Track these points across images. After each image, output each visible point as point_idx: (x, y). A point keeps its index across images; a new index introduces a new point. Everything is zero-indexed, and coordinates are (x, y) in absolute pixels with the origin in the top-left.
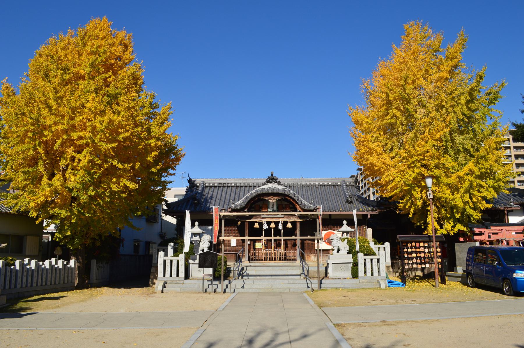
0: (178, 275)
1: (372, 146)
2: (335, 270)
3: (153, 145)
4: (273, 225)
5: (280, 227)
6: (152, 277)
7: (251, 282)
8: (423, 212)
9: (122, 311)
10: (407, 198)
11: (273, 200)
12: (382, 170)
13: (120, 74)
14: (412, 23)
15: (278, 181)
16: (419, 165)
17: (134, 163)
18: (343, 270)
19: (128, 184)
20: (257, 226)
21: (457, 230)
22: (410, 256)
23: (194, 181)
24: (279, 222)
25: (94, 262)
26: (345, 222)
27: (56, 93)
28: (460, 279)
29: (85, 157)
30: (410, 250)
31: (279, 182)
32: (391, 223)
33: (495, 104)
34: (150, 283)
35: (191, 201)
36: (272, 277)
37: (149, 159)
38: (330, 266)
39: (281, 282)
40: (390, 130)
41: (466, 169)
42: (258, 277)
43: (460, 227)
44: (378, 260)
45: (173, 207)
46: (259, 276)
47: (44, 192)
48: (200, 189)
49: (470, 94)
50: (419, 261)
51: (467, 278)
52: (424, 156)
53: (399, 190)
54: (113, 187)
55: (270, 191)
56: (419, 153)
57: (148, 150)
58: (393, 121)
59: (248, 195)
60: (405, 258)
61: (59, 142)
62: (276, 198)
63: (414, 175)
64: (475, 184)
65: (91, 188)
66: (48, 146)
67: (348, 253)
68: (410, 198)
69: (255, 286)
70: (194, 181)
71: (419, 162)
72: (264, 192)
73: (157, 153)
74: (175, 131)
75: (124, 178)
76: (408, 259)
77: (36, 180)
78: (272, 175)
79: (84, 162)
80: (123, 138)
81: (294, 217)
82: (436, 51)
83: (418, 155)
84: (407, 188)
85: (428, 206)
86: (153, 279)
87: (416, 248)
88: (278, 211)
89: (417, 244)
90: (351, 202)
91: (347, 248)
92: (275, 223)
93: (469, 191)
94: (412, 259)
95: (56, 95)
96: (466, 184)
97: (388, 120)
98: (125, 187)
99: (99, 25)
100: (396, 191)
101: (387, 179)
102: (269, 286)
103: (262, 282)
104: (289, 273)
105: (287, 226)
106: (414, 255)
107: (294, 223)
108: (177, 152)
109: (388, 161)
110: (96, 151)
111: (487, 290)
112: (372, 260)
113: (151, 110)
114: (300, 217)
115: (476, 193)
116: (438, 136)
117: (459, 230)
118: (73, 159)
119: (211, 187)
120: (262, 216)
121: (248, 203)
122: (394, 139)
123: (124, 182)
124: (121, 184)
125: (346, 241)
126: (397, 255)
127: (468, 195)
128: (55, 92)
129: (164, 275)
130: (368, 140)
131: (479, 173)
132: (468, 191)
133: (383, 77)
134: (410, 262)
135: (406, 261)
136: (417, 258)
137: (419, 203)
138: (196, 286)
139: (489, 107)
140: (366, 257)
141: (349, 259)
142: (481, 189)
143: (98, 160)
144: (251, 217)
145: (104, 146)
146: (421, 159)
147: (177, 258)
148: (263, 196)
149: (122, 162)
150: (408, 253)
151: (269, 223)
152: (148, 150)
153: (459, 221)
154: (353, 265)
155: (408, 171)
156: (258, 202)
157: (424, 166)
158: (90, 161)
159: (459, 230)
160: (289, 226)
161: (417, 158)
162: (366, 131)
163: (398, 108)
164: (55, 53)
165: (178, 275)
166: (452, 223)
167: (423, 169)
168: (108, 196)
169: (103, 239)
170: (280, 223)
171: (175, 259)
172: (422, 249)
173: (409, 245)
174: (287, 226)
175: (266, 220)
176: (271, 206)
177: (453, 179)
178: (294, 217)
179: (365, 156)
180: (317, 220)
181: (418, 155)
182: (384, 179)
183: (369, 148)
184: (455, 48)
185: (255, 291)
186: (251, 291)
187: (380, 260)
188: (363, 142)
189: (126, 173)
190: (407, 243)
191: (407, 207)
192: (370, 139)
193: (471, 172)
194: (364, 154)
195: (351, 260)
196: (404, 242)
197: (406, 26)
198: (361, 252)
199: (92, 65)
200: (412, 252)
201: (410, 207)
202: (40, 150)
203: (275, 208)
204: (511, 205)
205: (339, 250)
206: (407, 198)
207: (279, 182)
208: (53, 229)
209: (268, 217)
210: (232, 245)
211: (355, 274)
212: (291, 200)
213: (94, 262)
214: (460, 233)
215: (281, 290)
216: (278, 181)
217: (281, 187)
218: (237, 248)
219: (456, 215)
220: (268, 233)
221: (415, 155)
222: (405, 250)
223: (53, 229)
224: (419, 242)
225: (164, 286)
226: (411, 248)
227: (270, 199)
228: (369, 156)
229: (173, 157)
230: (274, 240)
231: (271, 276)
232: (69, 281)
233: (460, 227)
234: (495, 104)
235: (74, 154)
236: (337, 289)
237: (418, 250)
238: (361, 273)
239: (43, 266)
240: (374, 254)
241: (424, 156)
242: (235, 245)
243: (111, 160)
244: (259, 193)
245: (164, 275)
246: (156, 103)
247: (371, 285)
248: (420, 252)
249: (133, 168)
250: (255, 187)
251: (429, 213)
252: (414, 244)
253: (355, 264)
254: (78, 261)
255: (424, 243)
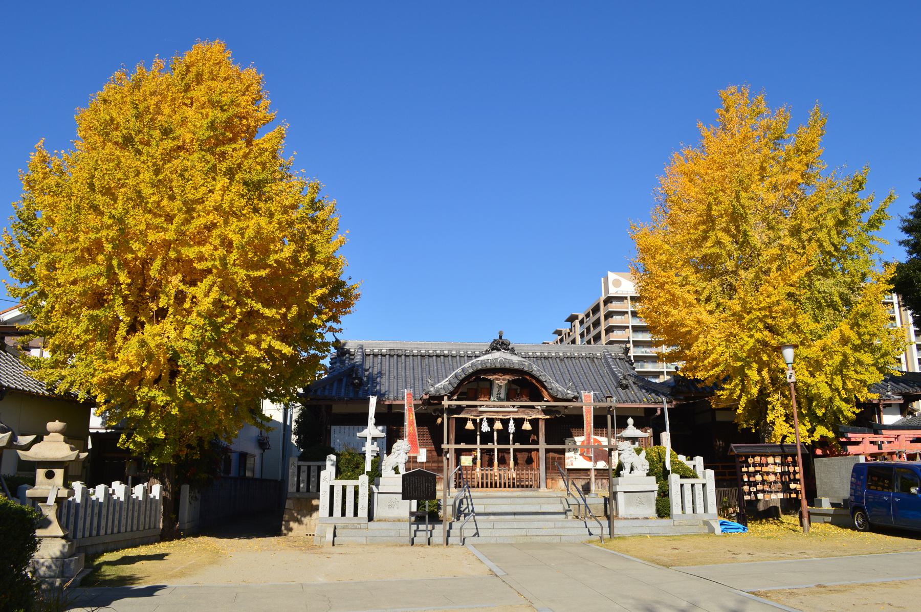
0: (356, 514)
1: (678, 291)
2: (628, 503)
3: (317, 276)
4: (498, 426)
5: (512, 428)
6: (286, 517)
7: (490, 525)
8: (759, 406)
9: (321, 580)
10: (737, 381)
11: (501, 381)
12: (695, 332)
13: (257, 145)
14: (733, 89)
15: (510, 347)
16: (760, 325)
17: (289, 309)
18: (641, 503)
19: (277, 345)
20: (470, 426)
21: (818, 436)
22: (752, 479)
23: (344, 344)
24: (509, 419)
25: (186, 489)
26: (630, 421)
27: (157, 172)
28: (829, 519)
29: (205, 295)
30: (751, 469)
31: (513, 349)
32: (704, 424)
33: (878, 228)
34: (283, 528)
35: (345, 380)
36: (517, 517)
37: (310, 300)
38: (621, 497)
39: (541, 524)
40: (708, 267)
41: (835, 334)
42: (492, 517)
43: (821, 431)
44: (704, 485)
45: (316, 391)
46: (494, 514)
47: (128, 353)
48: (358, 359)
49: (844, 211)
50: (767, 488)
51: (853, 517)
52: (771, 312)
53: (721, 367)
54: (250, 349)
55: (498, 366)
56: (762, 305)
57: (308, 286)
58: (716, 250)
59: (459, 370)
60: (744, 483)
61: (157, 264)
62: (507, 377)
63: (751, 342)
64: (852, 360)
65: (211, 351)
66: (139, 272)
67: (648, 475)
68: (742, 381)
69: (497, 533)
70: (344, 344)
71: (761, 320)
72: (489, 366)
73: (327, 291)
74: (346, 251)
75: (269, 335)
76: (750, 484)
77: (106, 332)
78: (500, 337)
79: (206, 304)
80: (276, 261)
81: (533, 413)
82: (777, 138)
83: (760, 309)
84: (739, 364)
85: (768, 395)
86: (288, 521)
87: (761, 465)
88: (508, 399)
89: (764, 460)
90: (625, 387)
91: (647, 465)
92: (474, 421)
93: (841, 371)
94: (755, 484)
95: (157, 175)
96: (838, 359)
97: (708, 248)
98: (270, 351)
99: (209, 52)
100: (716, 369)
101: (702, 349)
102: (524, 532)
103: (515, 525)
104: (543, 510)
105: (523, 428)
106: (758, 478)
107: (534, 422)
108: (349, 290)
109: (705, 317)
110: (227, 286)
111: (903, 536)
112: (693, 485)
113: (311, 212)
114: (546, 411)
115: (851, 374)
116: (794, 278)
117: (821, 436)
118: (180, 297)
119: (375, 356)
120: (480, 409)
121: (459, 385)
122: (715, 282)
123: (268, 341)
124: (264, 345)
125: (643, 453)
126: (729, 478)
127: (839, 377)
128: (155, 171)
129: (331, 514)
130: (672, 282)
131: (859, 342)
132: (840, 370)
133: (686, 177)
134: (753, 489)
135: (746, 488)
136: (763, 482)
137: (755, 391)
138: (393, 533)
139: (870, 234)
140: (684, 481)
141: (652, 484)
142: (859, 368)
143: (228, 301)
144: (460, 409)
145: (240, 274)
146: (765, 316)
147: (355, 482)
148: (485, 374)
149: (267, 304)
150: (749, 474)
151: (491, 422)
152: (308, 286)
153: (821, 421)
154: (659, 494)
155: (742, 335)
156: (475, 384)
157: (769, 328)
158: (217, 303)
159: (821, 436)
160: (527, 426)
161: (758, 313)
162: (666, 266)
163: (727, 231)
164: (141, 98)
165: (356, 514)
166: (808, 424)
167: (766, 333)
168: (240, 368)
169: (206, 447)
170: (512, 422)
171: (339, 484)
172: (771, 468)
173: (750, 460)
174: (523, 428)
175: (485, 416)
176: (495, 390)
177: (814, 351)
178: (536, 411)
179: (666, 308)
180: (609, 417)
181: (760, 309)
182: (698, 347)
183: (673, 295)
184: (809, 135)
185: (500, 541)
186: (493, 541)
187: (707, 485)
188: (664, 284)
189: (273, 326)
190: (747, 457)
191: (735, 396)
192: (676, 279)
193: (844, 341)
194: (664, 304)
195: (656, 487)
196: (741, 456)
197: (723, 94)
198: (674, 471)
199: (212, 126)
200: (756, 472)
201: (740, 396)
202: (123, 278)
203: (503, 396)
204: (889, 396)
205: (632, 469)
206: (737, 381)
207: (513, 349)
208: (99, 426)
209: (494, 410)
210: (419, 460)
211: (663, 511)
212: (534, 381)
213: (186, 489)
214: (824, 442)
215: (547, 539)
216: (510, 347)
217: (515, 359)
218: (427, 465)
219: (817, 411)
220: (503, 437)
221: (755, 309)
222: (744, 469)
223: (99, 426)
224: (767, 456)
225: (335, 535)
226: (754, 465)
227: (497, 379)
228: (671, 309)
229: (339, 299)
230: (498, 450)
231: (515, 514)
232: (152, 526)
233: (821, 431)
234: (878, 228)
235: (182, 287)
236: (642, 536)
237: (765, 469)
238: (676, 509)
239: (94, 498)
240: (695, 477)
241: (771, 312)
242: (424, 460)
243: (249, 300)
244: (480, 367)
245: (331, 514)
246: (320, 201)
247: (695, 530)
248: (768, 473)
249: (284, 316)
250: (470, 357)
251: (770, 407)
252: (757, 459)
253: (664, 494)
254: (164, 489)
255: (774, 456)
